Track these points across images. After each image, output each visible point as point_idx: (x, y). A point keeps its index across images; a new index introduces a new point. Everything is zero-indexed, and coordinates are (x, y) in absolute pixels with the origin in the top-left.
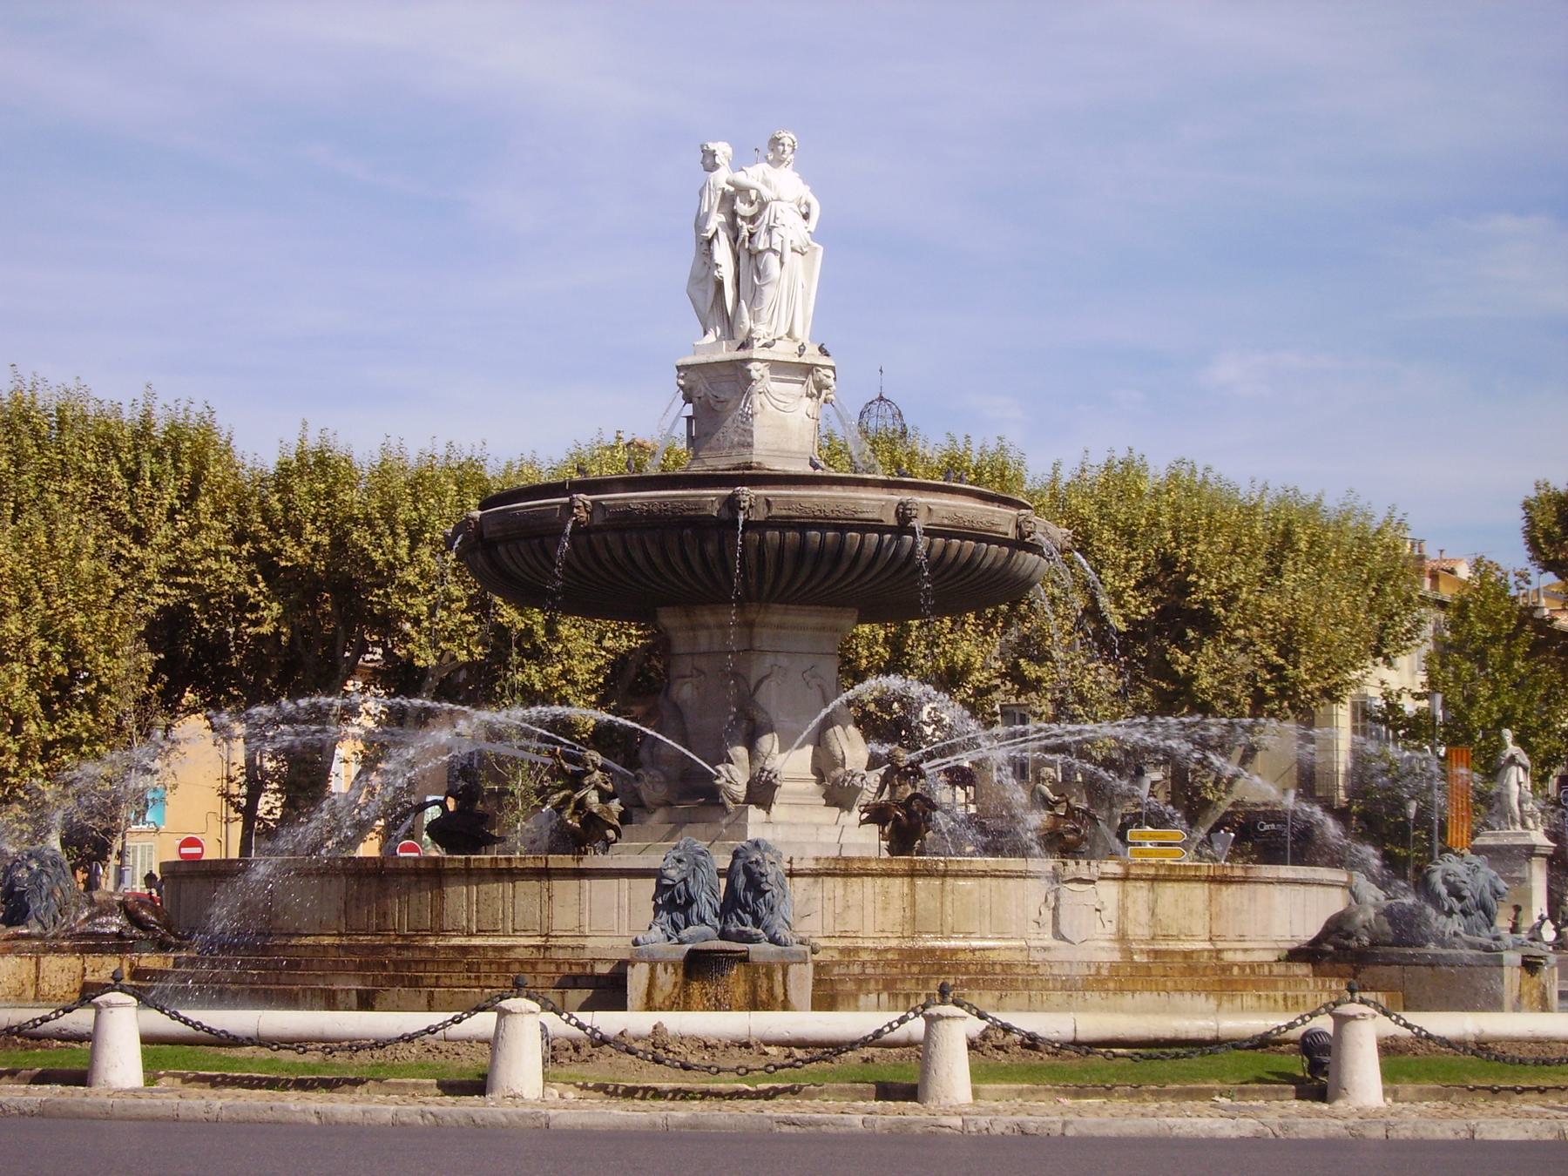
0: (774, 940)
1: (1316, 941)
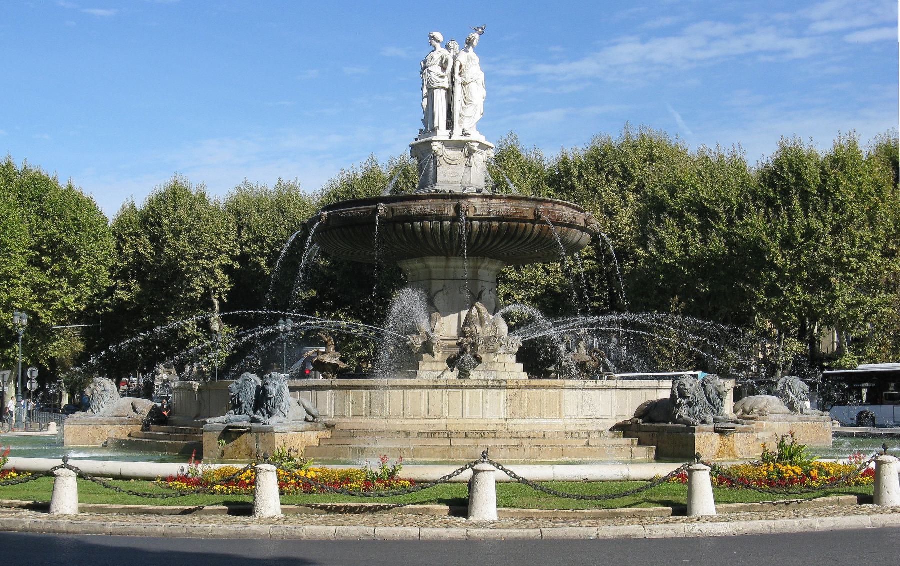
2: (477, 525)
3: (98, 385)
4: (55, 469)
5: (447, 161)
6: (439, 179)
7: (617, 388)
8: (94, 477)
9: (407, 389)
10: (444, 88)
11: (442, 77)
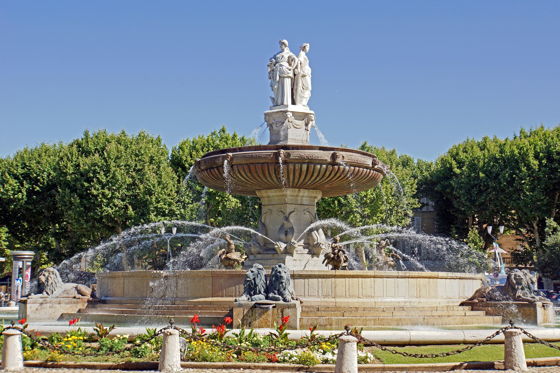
0: (285, 300)
1: (471, 299)
3: (51, 273)
5: (294, 125)
6: (289, 137)
7: (460, 278)
9: (347, 277)
10: (290, 77)
11: (290, 70)
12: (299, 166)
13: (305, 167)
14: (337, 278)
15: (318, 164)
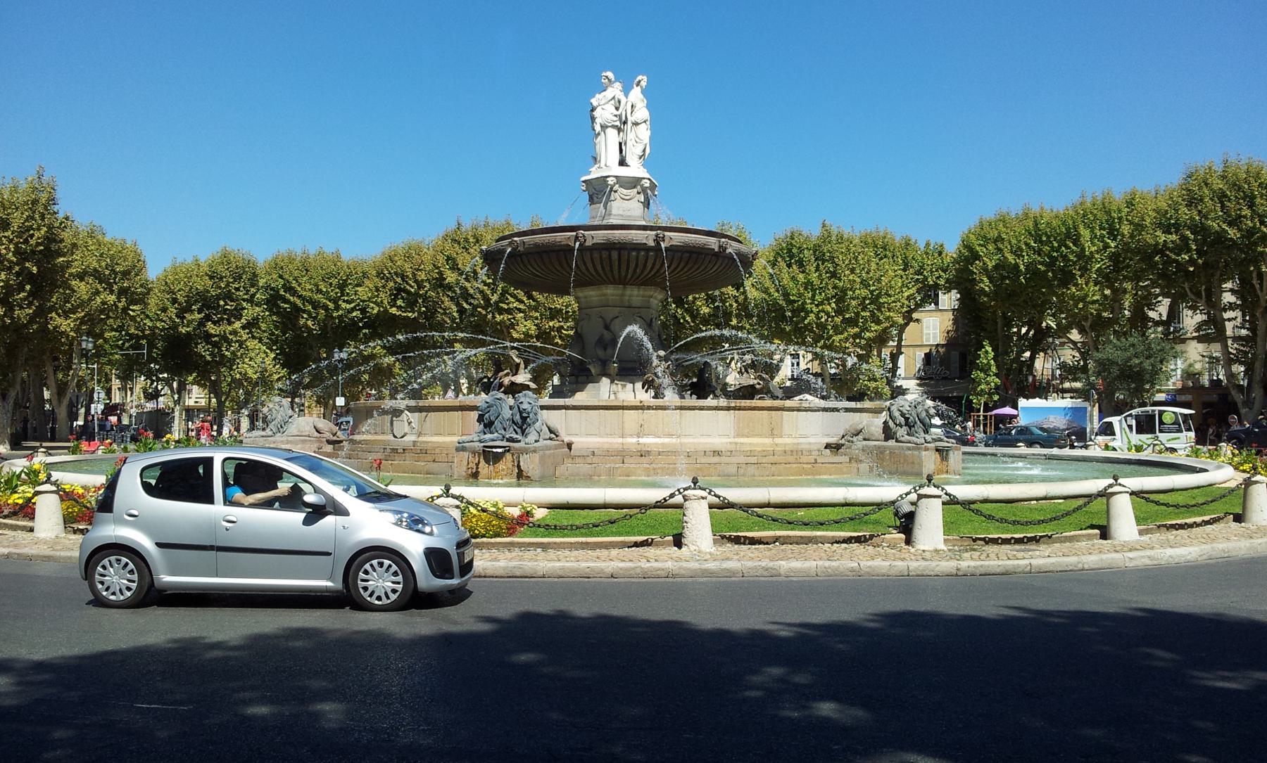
2: (922, 556)
4: (1105, 489)
8: (967, 504)
12: (607, 253)
13: (615, 255)
14: (626, 409)
15: (634, 249)
